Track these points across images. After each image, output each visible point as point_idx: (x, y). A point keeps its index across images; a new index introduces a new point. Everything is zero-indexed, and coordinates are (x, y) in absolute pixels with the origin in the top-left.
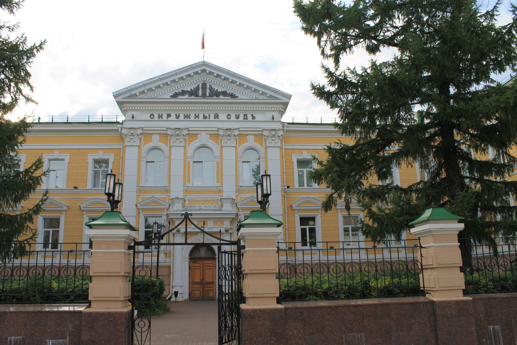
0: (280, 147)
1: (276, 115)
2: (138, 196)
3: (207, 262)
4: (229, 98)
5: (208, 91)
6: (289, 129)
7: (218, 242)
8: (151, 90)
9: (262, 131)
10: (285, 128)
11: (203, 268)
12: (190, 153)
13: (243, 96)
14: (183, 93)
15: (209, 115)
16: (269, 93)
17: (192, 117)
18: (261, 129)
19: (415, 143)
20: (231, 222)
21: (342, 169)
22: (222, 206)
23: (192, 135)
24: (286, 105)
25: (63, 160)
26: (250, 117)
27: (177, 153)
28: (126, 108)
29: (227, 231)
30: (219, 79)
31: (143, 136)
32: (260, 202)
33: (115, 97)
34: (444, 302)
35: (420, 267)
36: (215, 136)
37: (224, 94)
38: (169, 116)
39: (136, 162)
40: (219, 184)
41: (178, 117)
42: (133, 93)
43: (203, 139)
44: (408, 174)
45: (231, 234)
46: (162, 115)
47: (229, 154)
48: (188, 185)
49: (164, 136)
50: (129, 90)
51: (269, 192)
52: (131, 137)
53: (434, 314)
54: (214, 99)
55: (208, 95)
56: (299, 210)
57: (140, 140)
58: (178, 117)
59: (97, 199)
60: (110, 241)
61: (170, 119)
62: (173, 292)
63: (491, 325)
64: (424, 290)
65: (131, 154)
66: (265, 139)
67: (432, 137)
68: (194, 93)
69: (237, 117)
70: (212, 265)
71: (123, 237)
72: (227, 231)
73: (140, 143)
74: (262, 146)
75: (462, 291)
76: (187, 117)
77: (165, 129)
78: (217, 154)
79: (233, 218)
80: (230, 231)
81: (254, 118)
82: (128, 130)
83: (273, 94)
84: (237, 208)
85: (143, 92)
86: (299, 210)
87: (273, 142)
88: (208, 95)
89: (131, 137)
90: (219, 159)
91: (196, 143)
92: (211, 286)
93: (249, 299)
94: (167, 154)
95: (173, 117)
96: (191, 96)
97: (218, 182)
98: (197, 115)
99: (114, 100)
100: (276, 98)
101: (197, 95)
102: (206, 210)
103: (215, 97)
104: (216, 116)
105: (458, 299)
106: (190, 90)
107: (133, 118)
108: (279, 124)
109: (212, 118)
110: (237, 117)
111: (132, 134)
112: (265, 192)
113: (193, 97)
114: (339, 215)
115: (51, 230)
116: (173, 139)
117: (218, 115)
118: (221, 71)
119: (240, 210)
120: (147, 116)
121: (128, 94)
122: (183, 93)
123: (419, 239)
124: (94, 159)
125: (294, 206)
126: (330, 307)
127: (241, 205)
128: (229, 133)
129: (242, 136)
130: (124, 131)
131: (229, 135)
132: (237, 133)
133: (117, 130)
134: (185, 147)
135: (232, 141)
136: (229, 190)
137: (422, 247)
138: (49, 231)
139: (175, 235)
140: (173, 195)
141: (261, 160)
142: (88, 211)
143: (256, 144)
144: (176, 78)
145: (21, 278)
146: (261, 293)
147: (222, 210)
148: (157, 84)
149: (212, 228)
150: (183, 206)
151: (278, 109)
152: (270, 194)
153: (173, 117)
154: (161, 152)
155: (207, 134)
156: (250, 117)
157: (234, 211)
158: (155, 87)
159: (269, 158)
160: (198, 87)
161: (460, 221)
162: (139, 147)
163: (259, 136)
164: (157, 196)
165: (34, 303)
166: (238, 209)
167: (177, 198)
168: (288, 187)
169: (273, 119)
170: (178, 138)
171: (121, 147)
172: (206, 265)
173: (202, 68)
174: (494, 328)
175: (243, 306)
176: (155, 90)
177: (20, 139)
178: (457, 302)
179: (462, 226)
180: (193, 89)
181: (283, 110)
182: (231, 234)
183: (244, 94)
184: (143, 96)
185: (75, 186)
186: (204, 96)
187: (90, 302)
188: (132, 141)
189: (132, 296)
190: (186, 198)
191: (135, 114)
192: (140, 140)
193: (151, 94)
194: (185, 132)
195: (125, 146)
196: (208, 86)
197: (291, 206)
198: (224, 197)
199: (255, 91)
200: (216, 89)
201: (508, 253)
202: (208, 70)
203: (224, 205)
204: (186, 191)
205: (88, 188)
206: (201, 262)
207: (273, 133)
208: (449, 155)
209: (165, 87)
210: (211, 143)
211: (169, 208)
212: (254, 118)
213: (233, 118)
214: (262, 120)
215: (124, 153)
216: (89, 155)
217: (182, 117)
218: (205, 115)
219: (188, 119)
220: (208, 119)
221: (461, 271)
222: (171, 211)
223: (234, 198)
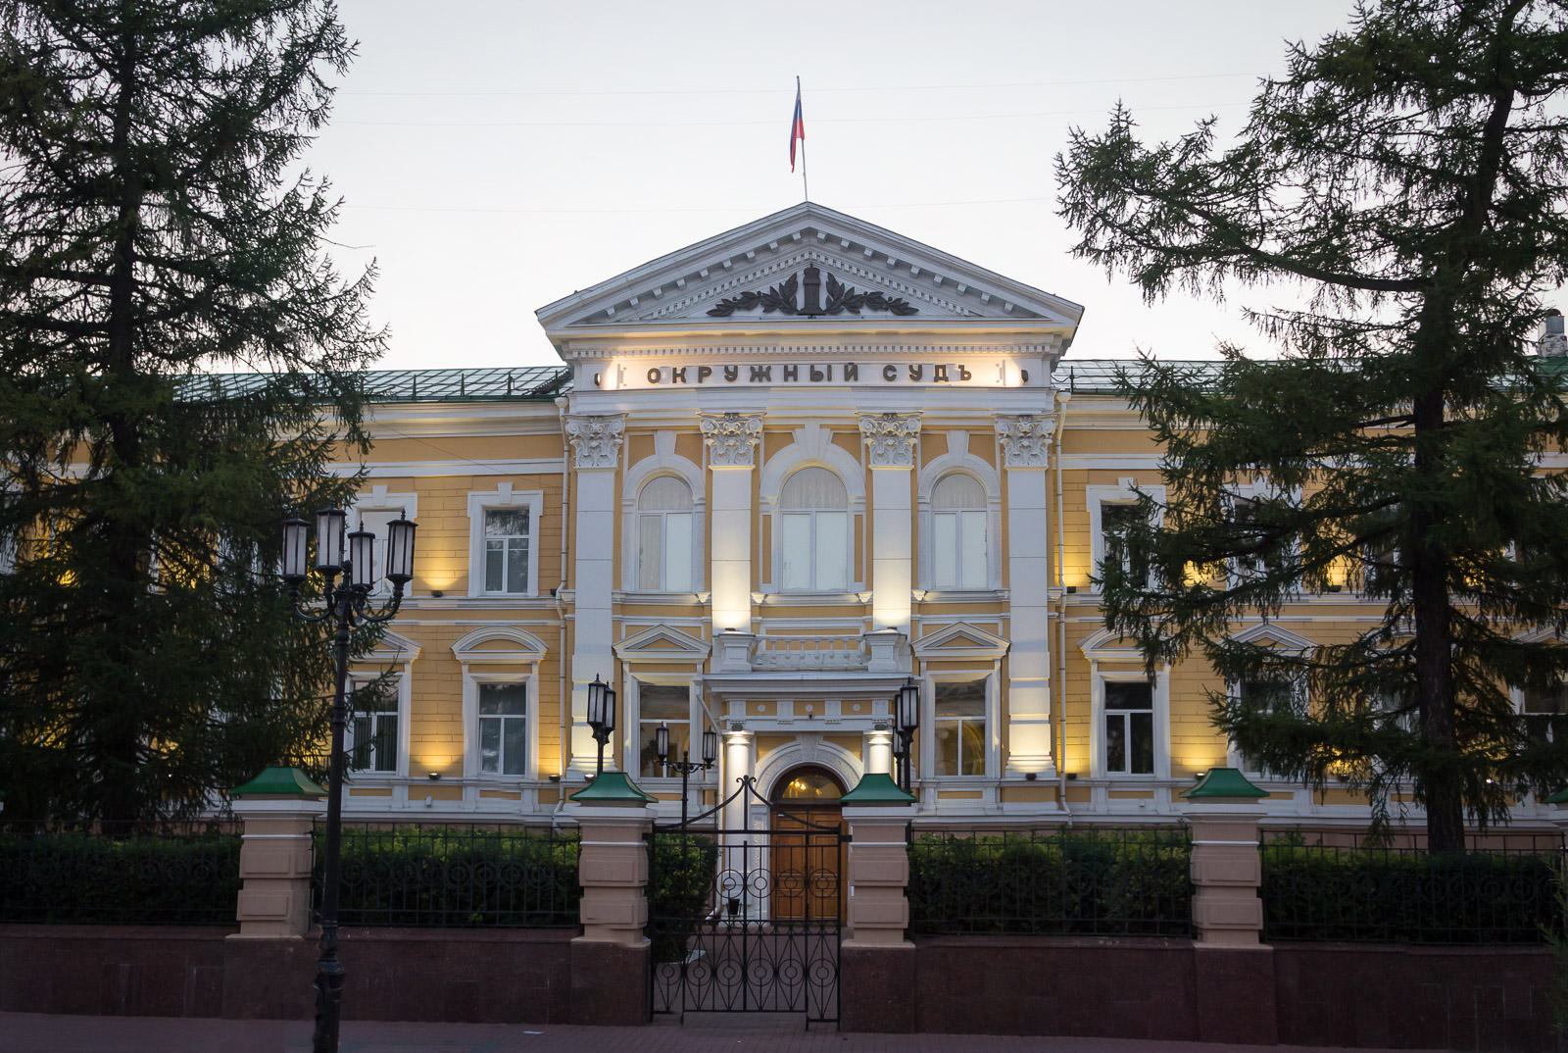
2: (617, 624)
4: (889, 313)
5: (824, 295)
7: (805, 828)
10: (1064, 410)
14: (749, 301)
15: (829, 367)
17: (777, 374)
28: (575, 355)
30: (857, 256)
33: (544, 323)
36: (848, 438)
37: (875, 301)
39: (610, 519)
40: (998, 586)
41: (731, 375)
55: (823, 306)
57: (621, 450)
61: (708, 382)
62: (726, 901)
65: (594, 492)
66: (1002, 447)
73: (620, 461)
84: (915, 658)
87: (1026, 454)
88: (823, 306)
89: (594, 444)
101: (789, 308)
103: (846, 314)
104: (851, 372)
106: (766, 291)
108: (1043, 396)
113: (777, 314)
115: (1127, 713)
117: (855, 367)
118: (860, 234)
119: (923, 665)
122: (749, 301)
124: (484, 507)
127: (926, 648)
130: (572, 427)
138: (1122, 717)
143: (974, 458)
144: (724, 257)
147: (866, 669)
149: (788, 722)
154: (685, 488)
157: (903, 669)
160: (792, 283)
166: (917, 661)
171: (563, 468)
173: (803, 225)
177: (1328, 576)
180: (777, 288)
183: (935, 300)
186: (812, 311)
187: (582, 927)
188: (596, 455)
189: (650, 921)
192: (621, 450)
196: (824, 278)
202: (824, 230)
209: (692, 285)
218: (817, 368)
220: (824, 382)
222: (716, 668)
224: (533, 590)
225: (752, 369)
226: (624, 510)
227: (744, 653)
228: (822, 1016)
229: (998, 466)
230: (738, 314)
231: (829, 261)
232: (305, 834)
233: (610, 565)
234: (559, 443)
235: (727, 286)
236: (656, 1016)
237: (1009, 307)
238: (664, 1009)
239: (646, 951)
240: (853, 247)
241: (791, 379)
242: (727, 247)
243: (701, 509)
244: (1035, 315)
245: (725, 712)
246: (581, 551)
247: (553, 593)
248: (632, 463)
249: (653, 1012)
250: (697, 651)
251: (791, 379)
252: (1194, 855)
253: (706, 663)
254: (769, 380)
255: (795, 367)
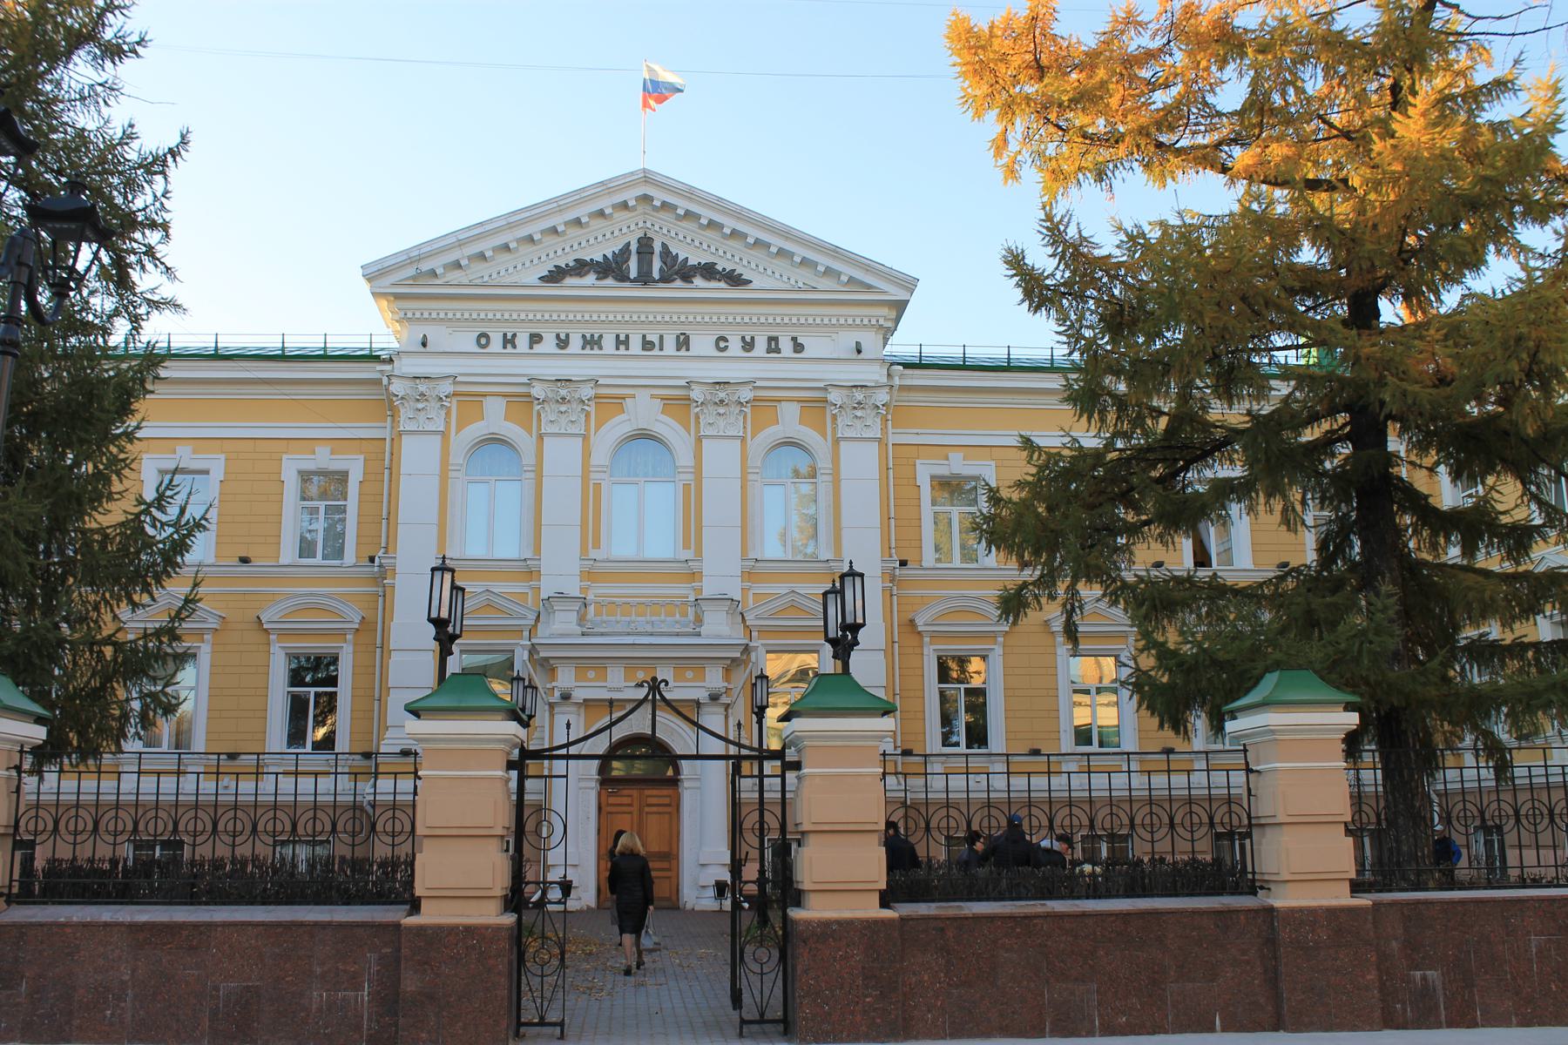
0: (879, 440)
1: (869, 340)
3: (655, 792)
4: (722, 284)
5: (657, 264)
6: (908, 382)
7: (733, 750)
8: (482, 256)
9: (825, 389)
11: (641, 811)
12: (600, 456)
13: (765, 278)
14: (581, 268)
15: (661, 337)
16: (848, 271)
17: (609, 343)
18: (821, 385)
19: (1276, 459)
20: (727, 670)
21: (1063, 523)
22: (699, 621)
23: (609, 402)
24: (900, 307)
25: (207, 472)
26: (786, 346)
27: (562, 456)
29: (714, 698)
31: (454, 400)
32: (833, 642)
34: (1301, 910)
35: (1246, 822)
37: (709, 271)
38: (535, 339)
39: (436, 481)
40: (689, 554)
41: (563, 343)
42: (425, 267)
43: (644, 412)
44: (1256, 544)
45: (727, 706)
46: (514, 335)
47: (722, 459)
48: (593, 554)
49: (522, 402)
50: (412, 258)
51: (860, 621)
52: (420, 406)
53: (1271, 942)
54: (677, 289)
55: (656, 275)
56: (935, 636)
57: (448, 414)
58: (563, 343)
59: (311, 594)
60: (469, 751)
61: (538, 348)
63: (1417, 968)
64: (1254, 880)
65: (418, 458)
67: (1325, 445)
68: (611, 268)
69: (748, 345)
70: (667, 801)
71: (500, 741)
72: (714, 698)
73: (447, 423)
74: (824, 435)
75: (1347, 884)
76: (591, 342)
77: (525, 380)
78: (685, 458)
79: (734, 660)
80: (724, 700)
81: (798, 348)
82: (409, 383)
83: (859, 275)
85: (457, 265)
86: (935, 636)
88: (656, 275)
89: (420, 406)
90: (690, 477)
91: (619, 427)
92: (665, 865)
93: (812, 895)
94: (529, 459)
95: (548, 344)
96: (605, 277)
97: (686, 546)
98: (622, 338)
99: (365, 287)
100: (869, 288)
101: (623, 277)
102: (652, 634)
103: (679, 283)
104: (683, 342)
105: (1334, 903)
106: (598, 258)
107: (424, 344)
108: (876, 367)
109: (670, 347)
110: (748, 345)
111: (422, 394)
112: (849, 620)
113: (610, 281)
114: (1059, 651)
116: (549, 413)
119: (755, 634)
120: (467, 342)
121: (411, 271)
122: (581, 268)
123: (1245, 751)
125: (920, 622)
126: (1012, 918)
128: (722, 395)
129: (763, 406)
130: (397, 387)
131: (722, 401)
132: (746, 394)
133: (378, 382)
134: (585, 438)
135: (732, 419)
136: (721, 573)
137: (1252, 771)
139: (557, 710)
140: (548, 588)
141: (820, 478)
142: (284, 634)
145: (79, 838)
146: (842, 879)
147: (699, 635)
148: (499, 240)
149: (619, 690)
150: (582, 619)
151: (874, 322)
152: (863, 625)
153: (548, 344)
155: (652, 396)
156: (786, 346)
158: (495, 249)
159: (844, 473)
160: (626, 249)
161: (1349, 707)
162: (444, 435)
163: (816, 405)
164: (499, 587)
165: (264, 904)
167: (561, 596)
168: (903, 563)
169: (859, 352)
170: (563, 408)
171: (387, 434)
172: (651, 801)
173: (640, 191)
174: (1424, 978)
175: (795, 913)
176: (492, 258)
178: (1333, 913)
179: (1353, 719)
180: (610, 256)
181: (889, 324)
182: (727, 706)
184: (455, 276)
185: (244, 555)
186: (645, 279)
190: (590, 597)
191: (432, 332)
192: (448, 414)
193: (478, 271)
194: (587, 392)
195: (400, 434)
196: (657, 248)
197: (912, 621)
198: (705, 594)
199: (805, 262)
200: (681, 258)
201: (1560, 779)
202: (659, 196)
203: (707, 618)
204: (589, 575)
205: (282, 561)
206: (635, 793)
207: (859, 395)
208: (1373, 496)
210: (667, 427)
211: (535, 626)
212: (798, 348)
213: (735, 347)
214: (828, 356)
215: (395, 455)
216: (285, 457)
217: (575, 345)
219: (596, 351)
220: (656, 352)
221: (1348, 832)
222: (544, 635)
223: (737, 597)
224: (350, 556)
225: (584, 336)
226: (451, 474)
227: (573, 617)
228: (762, 1015)
229: (829, 438)
230: (569, 281)
231: (666, 233)
232: (8, 769)
233: (435, 530)
234: (388, 406)
235: (560, 252)
236: (523, 1030)
237: (844, 279)
238: (757, 1017)
239: (510, 928)
240: (689, 215)
241: (622, 347)
242: (561, 210)
243: (532, 475)
244: (862, 284)
245: (553, 678)
246: (403, 515)
247: (372, 560)
248: (458, 430)
249: (520, 1024)
250: (525, 618)
251: (622, 347)
252: (1261, 785)
253: (532, 630)
254: (601, 348)
255: (627, 336)
